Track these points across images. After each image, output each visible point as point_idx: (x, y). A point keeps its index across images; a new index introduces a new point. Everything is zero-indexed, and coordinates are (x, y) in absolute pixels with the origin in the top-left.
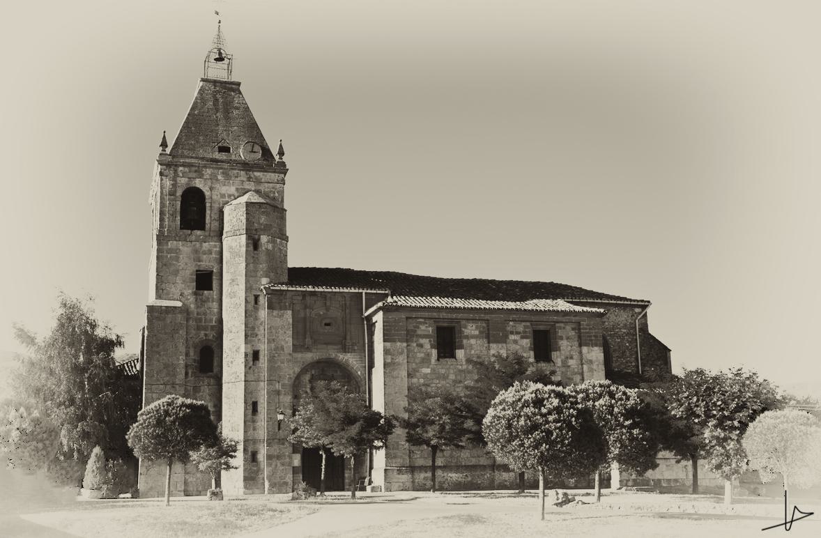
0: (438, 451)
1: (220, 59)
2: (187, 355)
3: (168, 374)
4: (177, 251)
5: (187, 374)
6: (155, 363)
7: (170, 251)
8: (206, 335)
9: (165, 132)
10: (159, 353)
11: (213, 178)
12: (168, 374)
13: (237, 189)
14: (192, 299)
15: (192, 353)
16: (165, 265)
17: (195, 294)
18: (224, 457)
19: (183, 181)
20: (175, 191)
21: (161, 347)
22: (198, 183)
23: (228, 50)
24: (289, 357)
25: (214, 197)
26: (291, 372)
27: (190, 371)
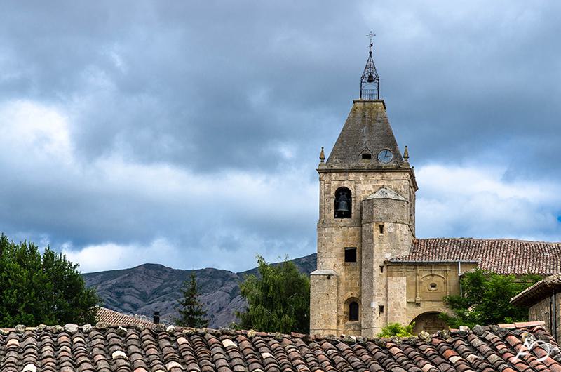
0: (377, 327)
1: (371, 80)
2: (338, 308)
3: (325, 323)
4: (332, 235)
5: (338, 322)
6: (317, 314)
7: (327, 235)
8: (352, 294)
9: (371, 53)
10: (319, 308)
11: (356, 182)
12: (325, 323)
13: (374, 187)
14: (342, 268)
15: (342, 307)
16: (324, 245)
17: (344, 265)
18: (299, 323)
19: (335, 185)
20: (330, 191)
21: (320, 303)
22: (346, 184)
23: (380, 71)
24: (404, 311)
25: (357, 193)
26: (405, 322)
27: (341, 320)
